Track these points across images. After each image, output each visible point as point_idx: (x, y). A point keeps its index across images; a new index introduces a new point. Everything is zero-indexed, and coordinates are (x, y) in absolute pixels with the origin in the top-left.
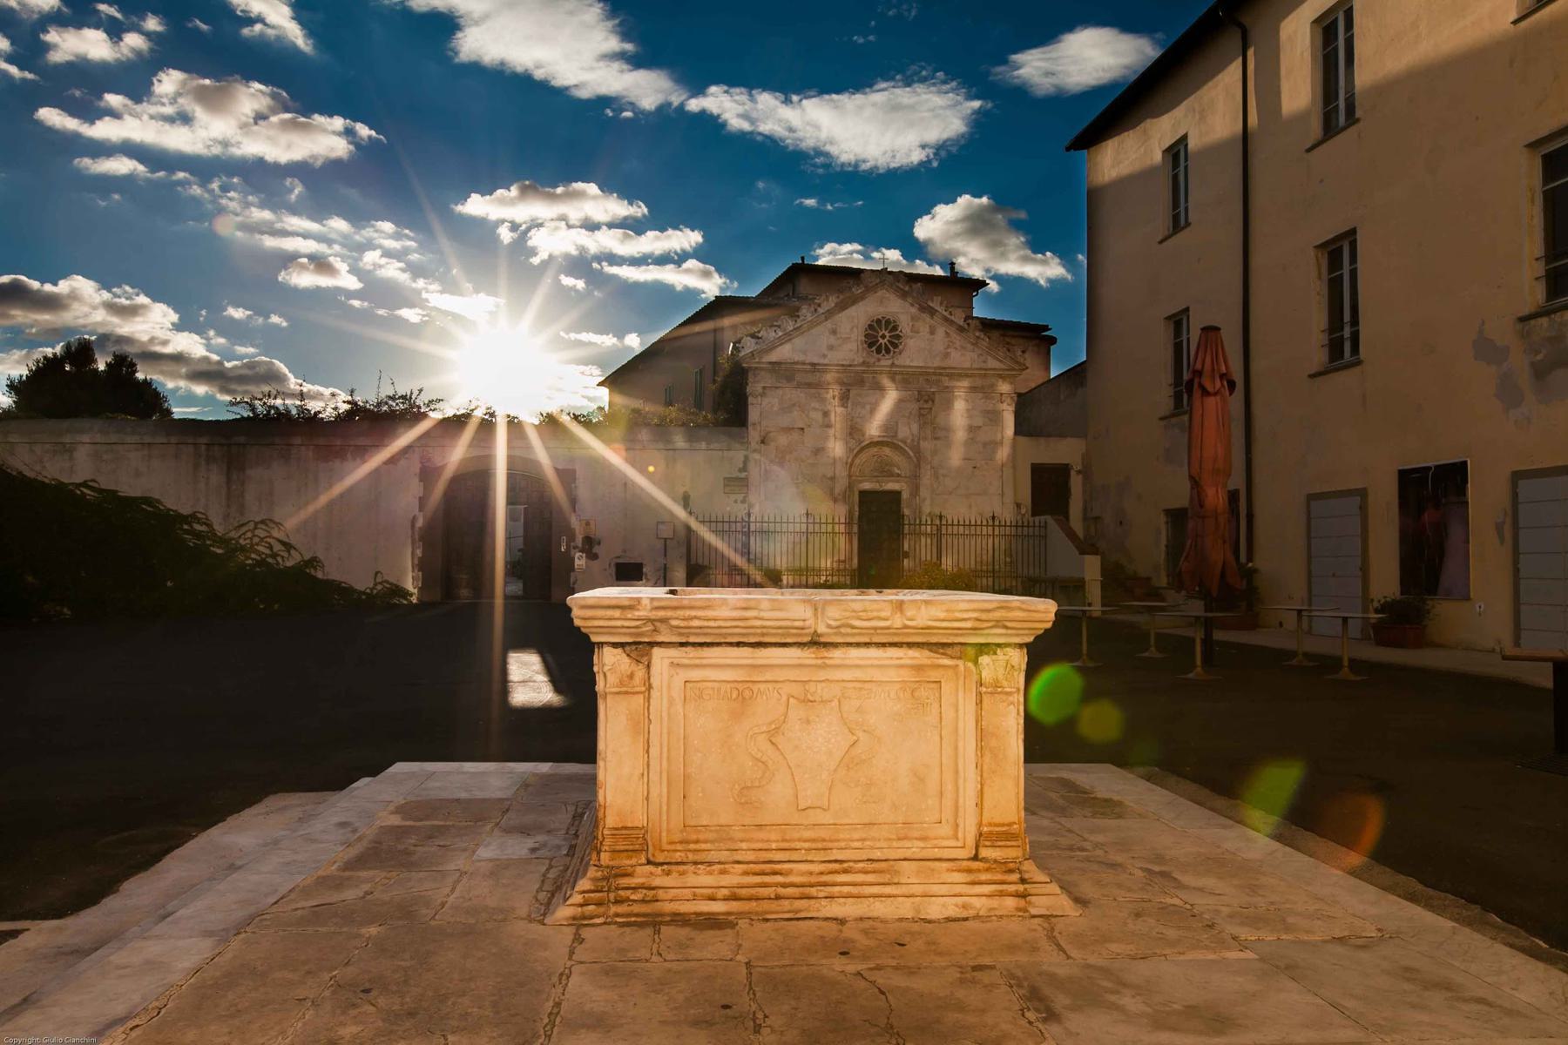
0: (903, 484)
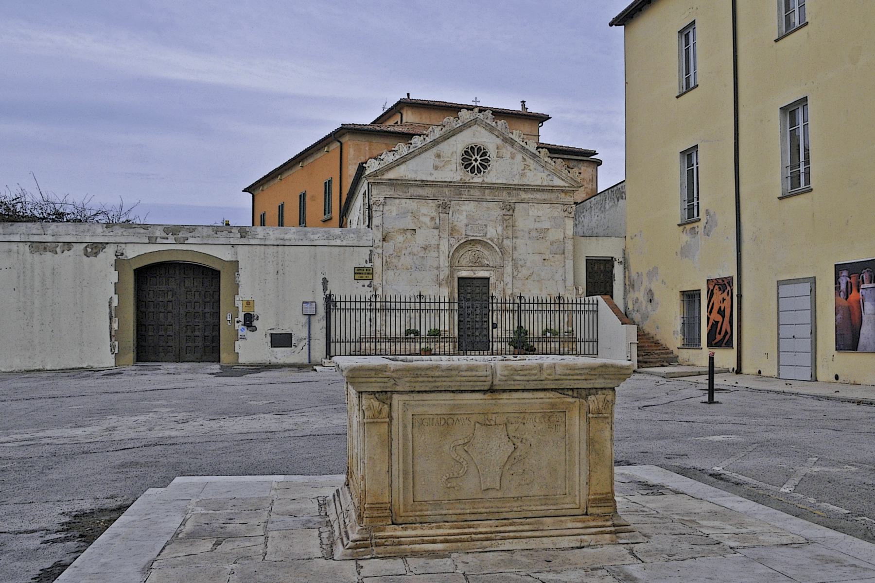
0: (492, 272)
